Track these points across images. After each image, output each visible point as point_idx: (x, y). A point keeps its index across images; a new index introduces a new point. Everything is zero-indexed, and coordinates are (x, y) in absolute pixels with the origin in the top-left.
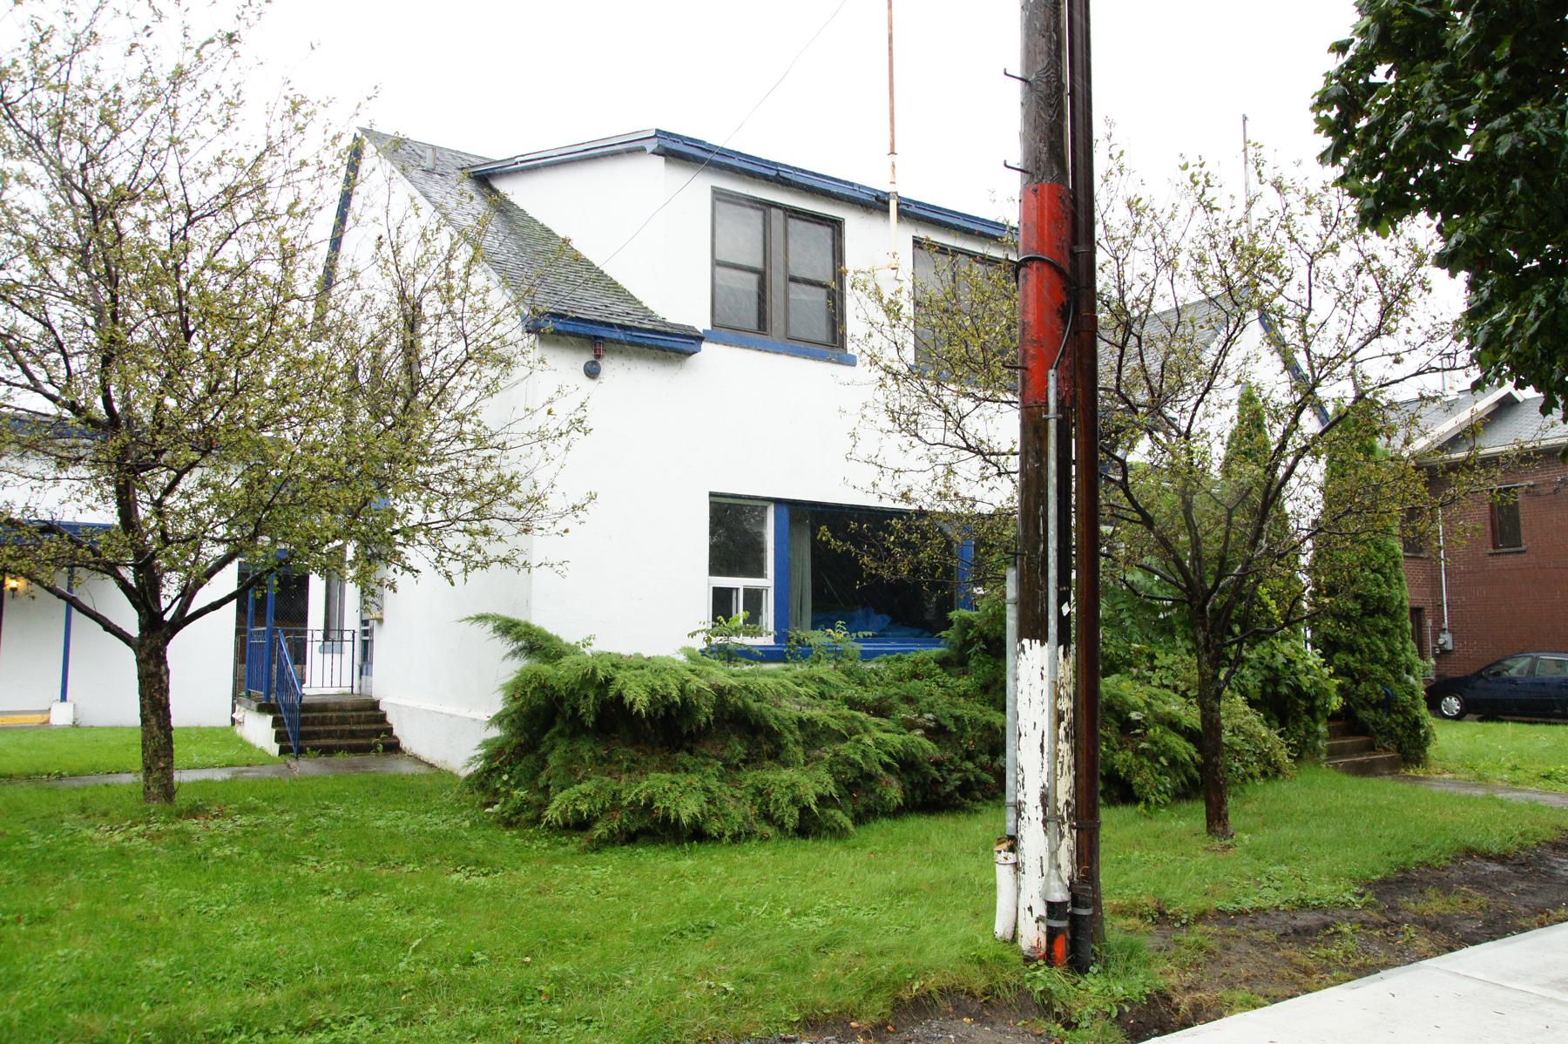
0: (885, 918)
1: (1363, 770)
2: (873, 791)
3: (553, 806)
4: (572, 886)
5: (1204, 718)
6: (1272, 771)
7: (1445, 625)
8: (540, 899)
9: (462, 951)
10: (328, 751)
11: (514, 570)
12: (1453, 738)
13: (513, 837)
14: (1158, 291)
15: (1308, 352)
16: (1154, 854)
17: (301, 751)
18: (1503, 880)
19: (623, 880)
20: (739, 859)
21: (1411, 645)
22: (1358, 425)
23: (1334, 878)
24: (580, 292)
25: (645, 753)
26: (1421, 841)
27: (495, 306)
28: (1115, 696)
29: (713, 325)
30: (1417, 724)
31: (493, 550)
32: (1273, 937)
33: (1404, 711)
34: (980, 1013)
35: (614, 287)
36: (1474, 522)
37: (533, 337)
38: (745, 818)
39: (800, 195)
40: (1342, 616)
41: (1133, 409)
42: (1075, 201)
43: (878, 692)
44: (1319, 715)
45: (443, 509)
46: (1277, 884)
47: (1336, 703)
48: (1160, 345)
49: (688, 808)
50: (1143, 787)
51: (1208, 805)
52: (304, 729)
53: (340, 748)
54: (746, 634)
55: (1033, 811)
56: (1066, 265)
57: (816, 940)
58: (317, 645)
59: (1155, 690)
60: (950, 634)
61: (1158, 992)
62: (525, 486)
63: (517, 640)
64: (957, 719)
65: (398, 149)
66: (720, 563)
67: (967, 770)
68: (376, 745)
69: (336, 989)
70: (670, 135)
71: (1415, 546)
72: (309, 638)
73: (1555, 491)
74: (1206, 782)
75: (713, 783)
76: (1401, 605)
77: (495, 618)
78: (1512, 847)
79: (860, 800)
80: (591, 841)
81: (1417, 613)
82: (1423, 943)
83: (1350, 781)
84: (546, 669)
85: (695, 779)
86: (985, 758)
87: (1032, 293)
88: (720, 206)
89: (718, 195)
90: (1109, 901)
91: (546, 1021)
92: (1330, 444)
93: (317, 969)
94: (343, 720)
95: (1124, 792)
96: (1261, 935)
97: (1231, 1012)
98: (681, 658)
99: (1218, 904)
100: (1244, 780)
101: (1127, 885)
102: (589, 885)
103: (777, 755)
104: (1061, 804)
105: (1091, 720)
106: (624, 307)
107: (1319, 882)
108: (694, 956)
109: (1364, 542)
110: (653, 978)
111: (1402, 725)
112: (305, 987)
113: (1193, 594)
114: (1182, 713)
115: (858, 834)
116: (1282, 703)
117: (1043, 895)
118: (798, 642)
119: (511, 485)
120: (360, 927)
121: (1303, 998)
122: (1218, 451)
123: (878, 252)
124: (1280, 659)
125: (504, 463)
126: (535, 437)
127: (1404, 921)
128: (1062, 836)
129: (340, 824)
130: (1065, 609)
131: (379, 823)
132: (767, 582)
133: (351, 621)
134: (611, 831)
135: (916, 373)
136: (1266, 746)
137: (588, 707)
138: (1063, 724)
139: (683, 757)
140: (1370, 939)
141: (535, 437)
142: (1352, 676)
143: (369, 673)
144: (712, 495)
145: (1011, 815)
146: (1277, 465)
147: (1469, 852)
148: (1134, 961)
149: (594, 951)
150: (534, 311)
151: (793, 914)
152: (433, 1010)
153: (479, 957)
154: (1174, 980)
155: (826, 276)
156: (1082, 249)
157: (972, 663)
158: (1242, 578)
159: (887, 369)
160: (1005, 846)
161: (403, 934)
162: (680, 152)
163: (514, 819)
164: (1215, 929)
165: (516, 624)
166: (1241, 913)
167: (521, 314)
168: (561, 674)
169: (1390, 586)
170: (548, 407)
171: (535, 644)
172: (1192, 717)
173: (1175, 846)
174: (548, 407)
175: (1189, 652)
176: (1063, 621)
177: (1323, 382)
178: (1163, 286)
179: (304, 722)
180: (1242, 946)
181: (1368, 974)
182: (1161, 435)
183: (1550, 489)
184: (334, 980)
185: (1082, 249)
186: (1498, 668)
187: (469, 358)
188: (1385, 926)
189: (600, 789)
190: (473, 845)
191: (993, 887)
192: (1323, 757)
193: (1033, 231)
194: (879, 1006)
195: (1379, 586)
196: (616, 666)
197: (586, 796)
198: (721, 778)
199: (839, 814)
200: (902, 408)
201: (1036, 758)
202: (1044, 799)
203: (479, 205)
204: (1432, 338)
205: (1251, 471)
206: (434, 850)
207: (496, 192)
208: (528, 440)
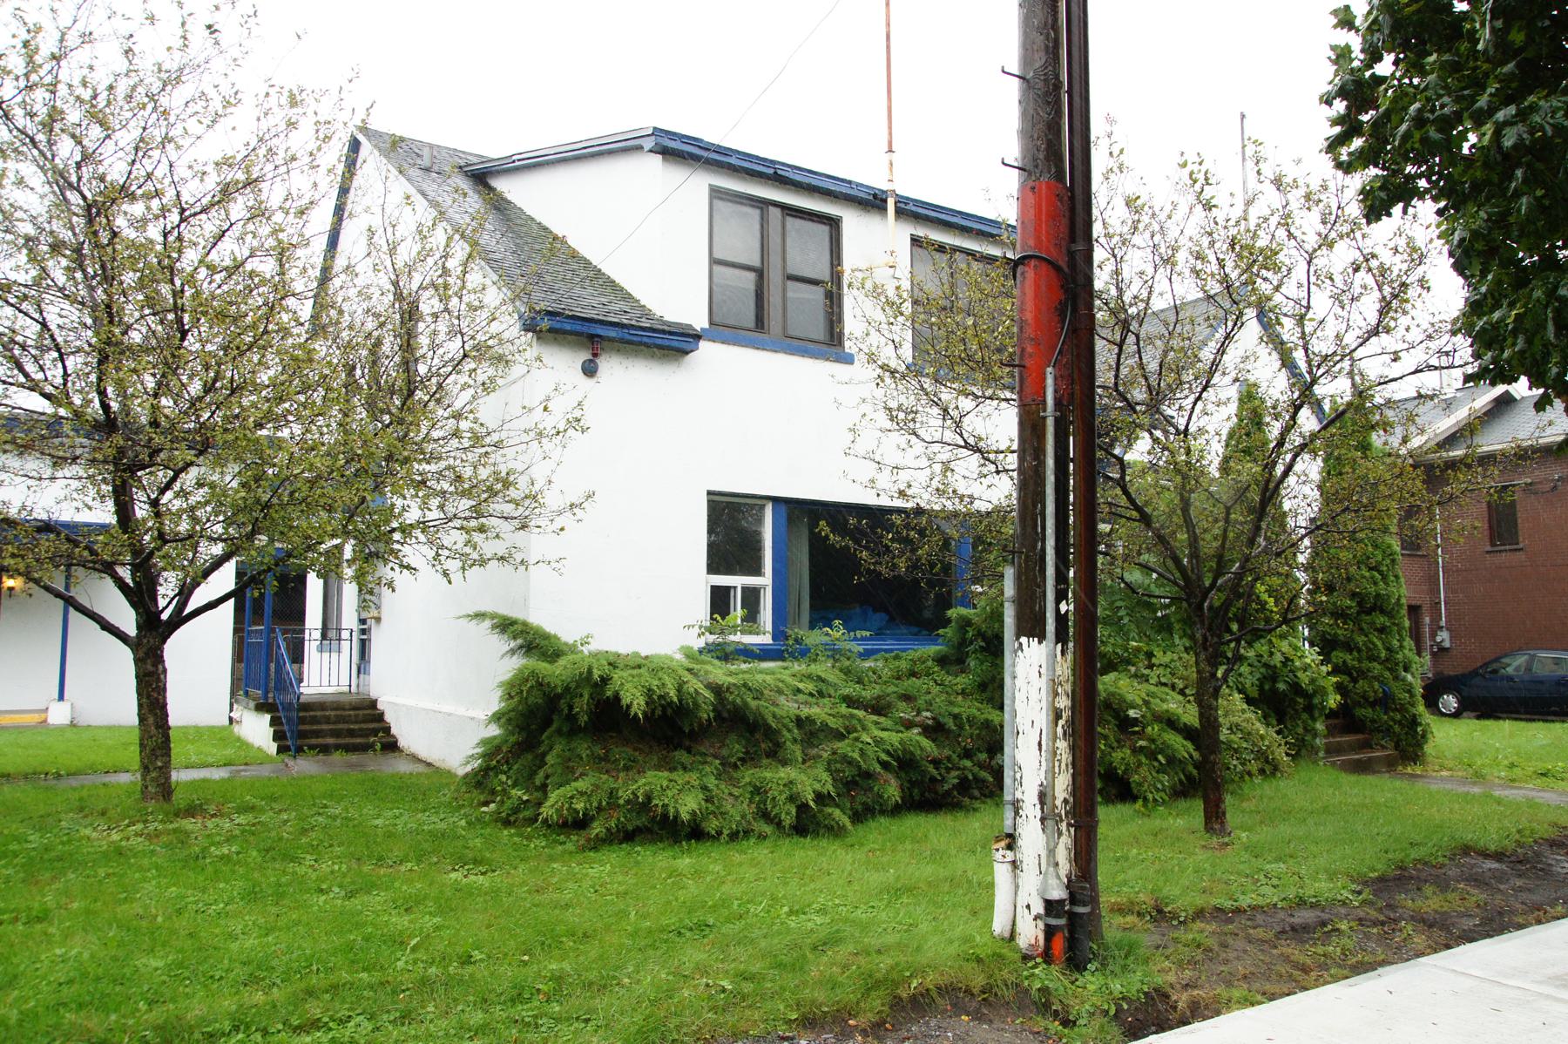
1: (1361, 768)
2: (871, 789)
3: (548, 804)
5: (1201, 715)
6: (1270, 769)
7: (1443, 623)
8: (538, 898)
10: (325, 750)
11: (511, 568)
12: (1450, 735)
13: (511, 836)
14: (1157, 289)
16: (1151, 852)
17: (299, 750)
18: (1501, 877)
20: (737, 858)
22: (1353, 424)
23: (1332, 876)
26: (1418, 838)
27: (493, 307)
28: (1113, 694)
29: (711, 323)
30: (1414, 722)
31: (489, 547)
32: (1270, 935)
33: (1402, 709)
34: (978, 1011)
36: (1471, 519)
37: (530, 335)
38: (743, 816)
40: (1339, 614)
41: (1131, 406)
42: (1072, 198)
45: (441, 507)
46: (1275, 881)
49: (688, 805)
50: (1140, 784)
55: (1031, 809)
56: (1063, 263)
58: (315, 644)
59: (1153, 688)
60: (948, 632)
62: (523, 482)
63: (515, 638)
64: (956, 717)
65: (394, 147)
66: (719, 560)
67: (965, 768)
71: (1413, 545)
74: (1205, 781)
75: (711, 782)
77: (493, 616)
78: (1509, 845)
80: (589, 840)
81: (1414, 610)
82: (1419, 940)
83: (1348, 779)
84: (543, 667)
85: (693, 777)
86: (983, 756)
87: (1030, 292)
88: (718, 204)
89: (716, 194)
90: (1106, 899)
95: (1122, 790)
96: (1259, 933)
97: (1229, 1009)
98: (679, 656)
100: (1242, 777)
101: (1125, 883)
102: (586, 884)
103: (776, 753)
104: (1058, 802)
105: (1089, 718)
106: (622, 305)
108: (692, 955)
110: (654, 975)
111: (1400, 722)
113: (1191, 591)
114: (1180, 711)
116: (1280, 700)
117: (1041, 892)
118: (796, 640)
120: (358, 926)
121: (1301, 996)
123: (875, 250)
124: (1278, 658)
127: (1401, 918)
128: (1060, 834)
130: (1063, 607)
131: (377, 822)
132: (765, 581)
133: (349, 619)
135: (914, 371)
137: (582, 705)
138: (1061, 722)
139: (682, 756)
140: (1367, 936)
142: (1350, 675)
144: (709, 493)
147: (1466, 850)
151: (791, 912)
152: (431, 1008)
153: (477, 955)
154: (1171, 978)
155: (821, 271)
158: (1239, 576)
160: (1003, 844)
162: (678, 151)
164: (1213, 927)
165: (513, 623)
166: (1238, 911)
168: (557, 672)
169: (1387, 584)
171: (533, 642)
172: (1190, 715)
173: (1173, 844)
175: (1187, 650)
176: (1061, 619)
178: (1161, 284)
179: (302, 721)
180: (1240, 944)
182: (1158, 433)
183: (1548, 487)
184: (333, 978)
185: (1080, 247)
186: (1495, 666)
191: (991, 885)
192: (1321, 754)
193: (1031, 228)
194: (877, 1003)
195: (1375, 583)
197: (582, 794)
199: (837, 813)
202: (1042, 797)
203: (474, 202)
208: (525, 438)
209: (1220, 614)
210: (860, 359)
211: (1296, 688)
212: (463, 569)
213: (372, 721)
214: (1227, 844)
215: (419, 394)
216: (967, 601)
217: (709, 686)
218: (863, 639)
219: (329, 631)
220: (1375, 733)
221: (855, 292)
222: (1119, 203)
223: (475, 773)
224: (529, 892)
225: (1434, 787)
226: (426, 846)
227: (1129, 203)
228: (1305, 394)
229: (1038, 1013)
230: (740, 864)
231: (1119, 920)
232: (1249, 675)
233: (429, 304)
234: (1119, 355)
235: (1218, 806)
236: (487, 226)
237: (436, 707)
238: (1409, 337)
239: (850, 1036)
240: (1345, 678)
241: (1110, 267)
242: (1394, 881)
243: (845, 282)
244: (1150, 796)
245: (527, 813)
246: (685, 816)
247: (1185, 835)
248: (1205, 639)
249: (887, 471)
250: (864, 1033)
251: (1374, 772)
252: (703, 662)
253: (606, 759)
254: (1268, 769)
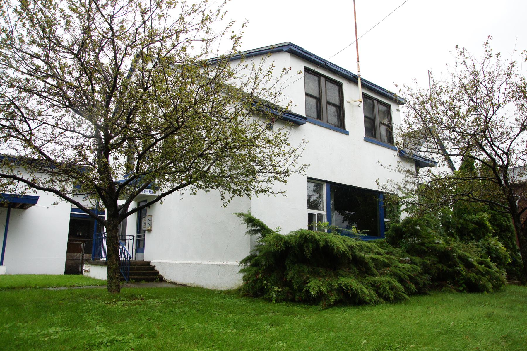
53: (142, 279)
94: (138, 269)
111: (520, 270)
132: (324, 212)
195: (506, 222)
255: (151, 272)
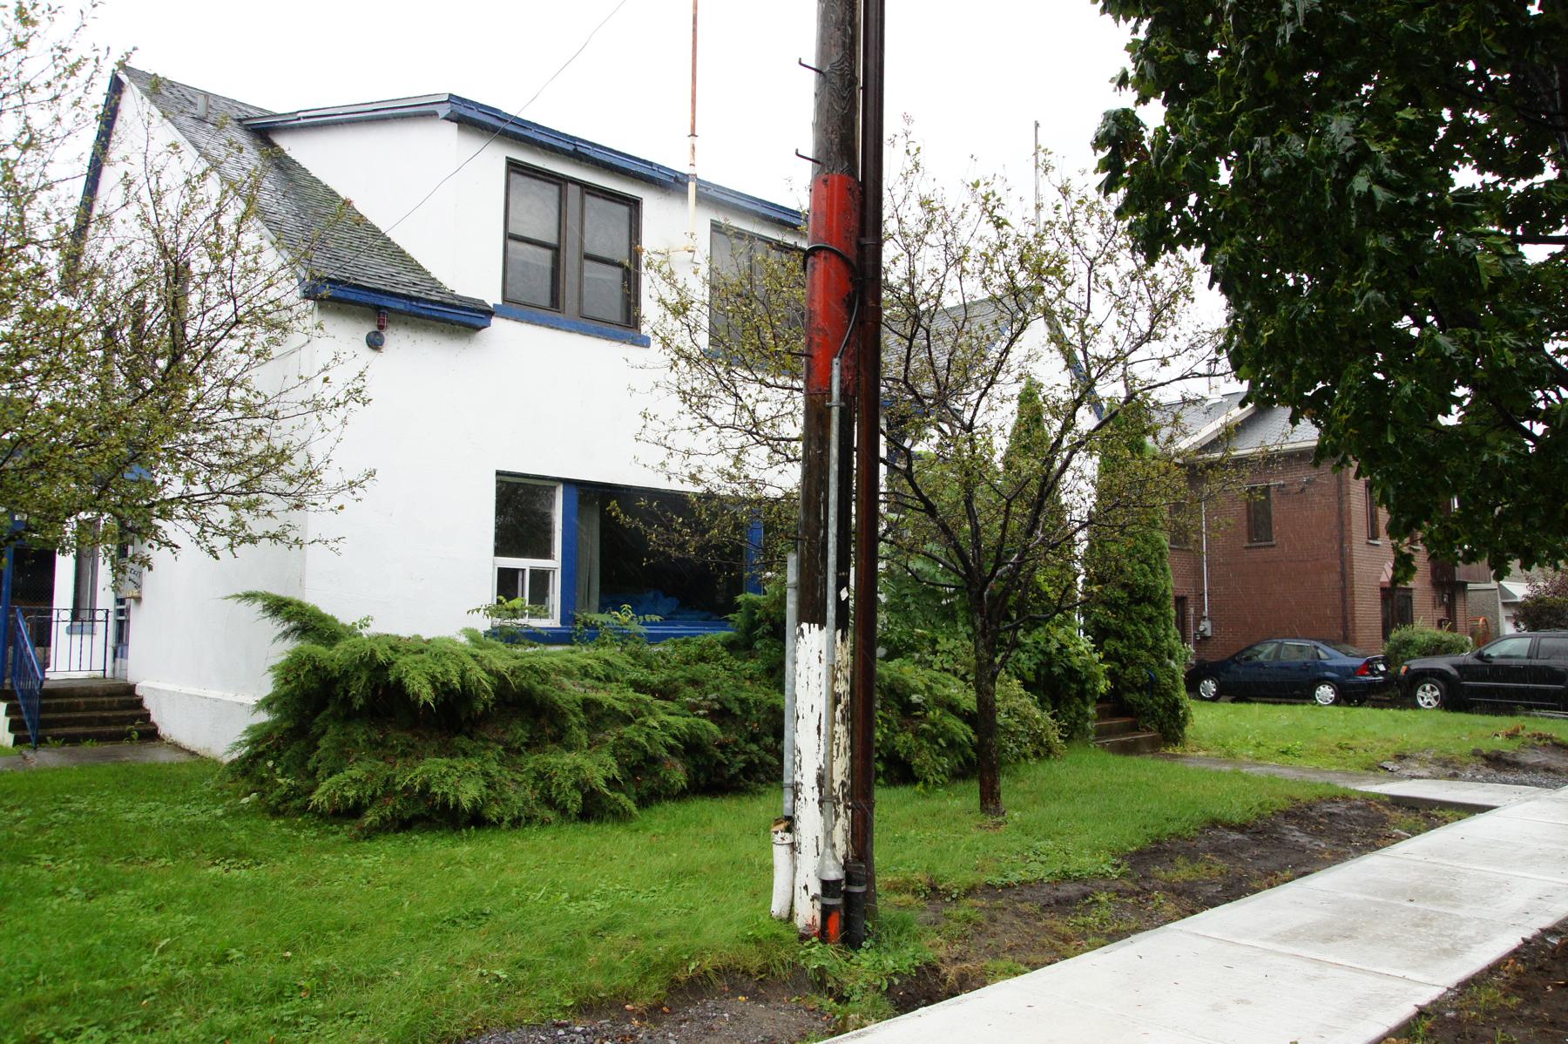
0: (664, 901)
1: (1127, 749)
2: (657, 774)
3: (319, 791)
4: (341, 875)
5: (979, 700)
6: (1044, 751)
7: (1206, 613)
8: (305, 891)
9: (215, 949)
10: (73, 740)
11: (285, 547)
12: (1208, 718)
13: (280, 827)
14: (948, 286)
15: (1085, 353)
16: (928, 833)
17: (41, 741)
18: (1240, 847)
19: (396, 868)
20: (519, 844)
21: (1174, 631)
22: (1129, 422)
23: (1095, 850)
24: (363, 259)
25: (421, 737)
26: (1174, 814)
27: (269, 269)
28: (897, 679)
29: (504, 299)
30: (1176, 706)
31: (256, 525)
32: (1036, 909)
33: (1166, 694)
34: (755, 991)
35: (400, 255)
36: (1234, 516)
37: (310, 302)
38: (526, 803)
39: (563, 160)
40: (1112, 605)
41: (919, 399)
42: (863, 193)
43: (664, 675)
44: (1089, 698)
45: (207, 482)
46: (1043, 858)
47: (1103, 686)
48: (947, 339)
49: (470, 793)
50: (921, 767)
51: (982, 783)
52: (43, 716)
53: (86, 737)
54: (531, 616)
55: (810, 792)
56: (852, 255)
57: (593, 924)
58: (63, 627)
59: (936, 674)
60: (737, 617)
61: (927, 964)
62: (299, 460)
63: (288, 620)
64: (742, 701)
65: (155, 87)
66: (506, 542)
67: (752, 752)
68: (129, 734)
69: (63, 1000)
70: (463, 100)
71: (1180, 537)
72: (55, 618)
73: (1303, 490)
74: (982, 764)
75: (493, 768)
76: (1165, 595)
77: (265, 596)
78: (1251, 817)
79: (644, 783)
80: (361, 829)
81: (1180, 601)
82: (1169, 908)
83: (1115, 760)
84: (321, 651)
85: (474, 763)
86: (770, 740)
87: (819, 284)
88: (515, 178)
89: (513, 166)
90: (881, 880)
91: (306, 1018)
92: (1102, 441)
93: (41, 978)
94: (91, 707)
95: (902, 773)
96: (1025, 907)
97: (995, 980)
98: (463, 639)
99: (986, 878)
100: (1017, 760)
101: (902, 863)
102: (359, 874)
103: (561, 739)
104: (836, 785)
105: (866, 701)
106: (411, 277)
107: (1081, 855)
108: (467, 943)
109: (1132, 535)
110: (422, 969)
112: (24, 999)
113: (972, 581)
114: (961, 696)
115: (643, 816)
116: (1056, 684)
117: (819, 873)
118: (585, 624)
119: (283, 456)
120: (98, 929)
121: (1061, 964)
122: (1001, 444)
123: (674, 235)
124: (1054, 645)
125: (275, 433)
126: (309, 406)
127: (1155, 888)
128: (837, 816)
129: (83, 818)
130: (844, 594)
131: (131, 816)
132: (554, 563)
133: (105, 599)
134: (383, 818)
135: (709, 357)
136: (1039, 728)
137: (358, 689)
138: (840, 707)
139: (462, 741)
140: (1124, 906)
141: (309, 406)
142: (1120, 661)
143: (124, 656)
144: (498, 473)
145: (788, 796)
146: (1054, 459)
147: (1215, 823)
148: (905, 935)
149: (362, 943)
150: (312, 276)
151: (571, 899)
152: (178, 1013)
153: (235, 954)
154: (942, 952)
155: (622, 256)
156: (868, 241)
157: (758, 645)
158: (1018, 566)
159: (679, 351)
160: (782, 826)
161: (148, 935)
162: (475, 120)
163: (281, 808)
164: (984, 902)
165: (288, 603)
166: (1008, 887)
167: (298, 276)
168: (335, 656)
169: (1155, 576)
170: (324, 375)
171: (306, 623)
172: (969, 700)
173: (949, 825)
174: (324, 375)
175: (969, 637)
176: (841, 606)
177: (1098, 382)
178: (952, 282)
179: (45, 709)
180: (1007, 918)
181: (1121, 938)
182: (945, 427)
183: (1297, 488)
184: (62, 988)
185: (868, 241)
186: (1248, 653)
187: (238, 322)
188: (1138, 894)
189: (372, 774)
190: (234, 836)
191: (771, 868)
192: (1092, 737)
193: (822, 221)
194: (655, 988)
195: (1145, 575)
196: (394, 649)
197: (355, 781)
198: (501, 762)
199: (623, 798)
200: (693, 390)
201: (813, 741)
202: (821, 780)
203: (251, 157)
204: (1193, 346)
205: (1029, 465)
206: (187, 843)
207: (273, 145)
208: (302, 409)
209: (999, 600)
210: (656, 345)
211: (1071, 672)
212: (231, 546)
213: (129, 708)
214: (1000, 824)
215: (187, 359)
216: (758, 589)
217: (490, 672)
218: (653, 623)
219: (81, 612)
220: (1140, 716)
221: (652, 272)
222: (914, 201)
223: (242, 761)
224: (296, 885)
225: (1191, 766)
226: (182, 839)
227: (925, 203)
228: (1085, 390)
229: (814, 990)
230: (522, 851)
231: (895, 898)
232: (1026, 661)
233: (200, 263)
234: (909, 349)
235: (993, 787)
236: (266, 183)
237: (202, 692)
238: (1176, 345)
239: (1415, 1040)
240: (1116, 665)
241: (903, 264)
242: (1155, 852)
243: (644, 261)
244: (931, 779)
245: (298, 802)
246: (466, 804)
247: (961, 816)
248: (984, 626)
249: (678, 458)
250: (641, 1017)
251: (1139, 753)
252: (488, 647)
253: (381, 744)
254: (1042, 751)
255: (135, 712)
